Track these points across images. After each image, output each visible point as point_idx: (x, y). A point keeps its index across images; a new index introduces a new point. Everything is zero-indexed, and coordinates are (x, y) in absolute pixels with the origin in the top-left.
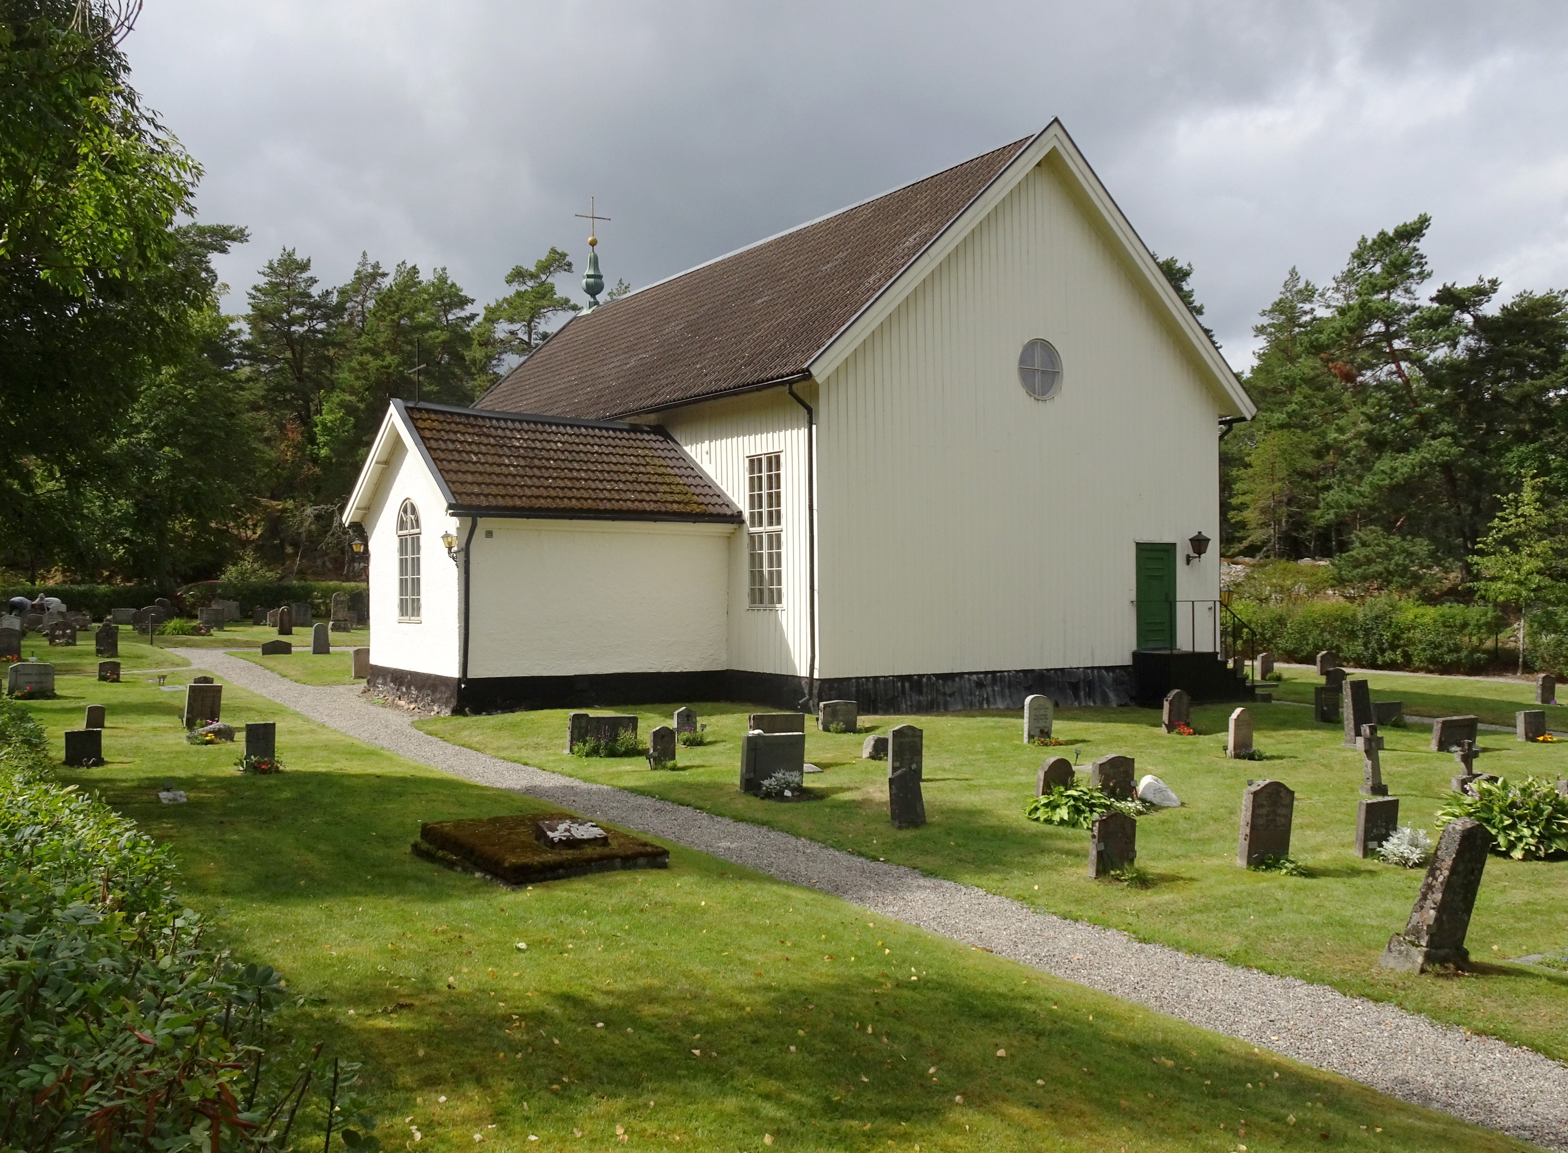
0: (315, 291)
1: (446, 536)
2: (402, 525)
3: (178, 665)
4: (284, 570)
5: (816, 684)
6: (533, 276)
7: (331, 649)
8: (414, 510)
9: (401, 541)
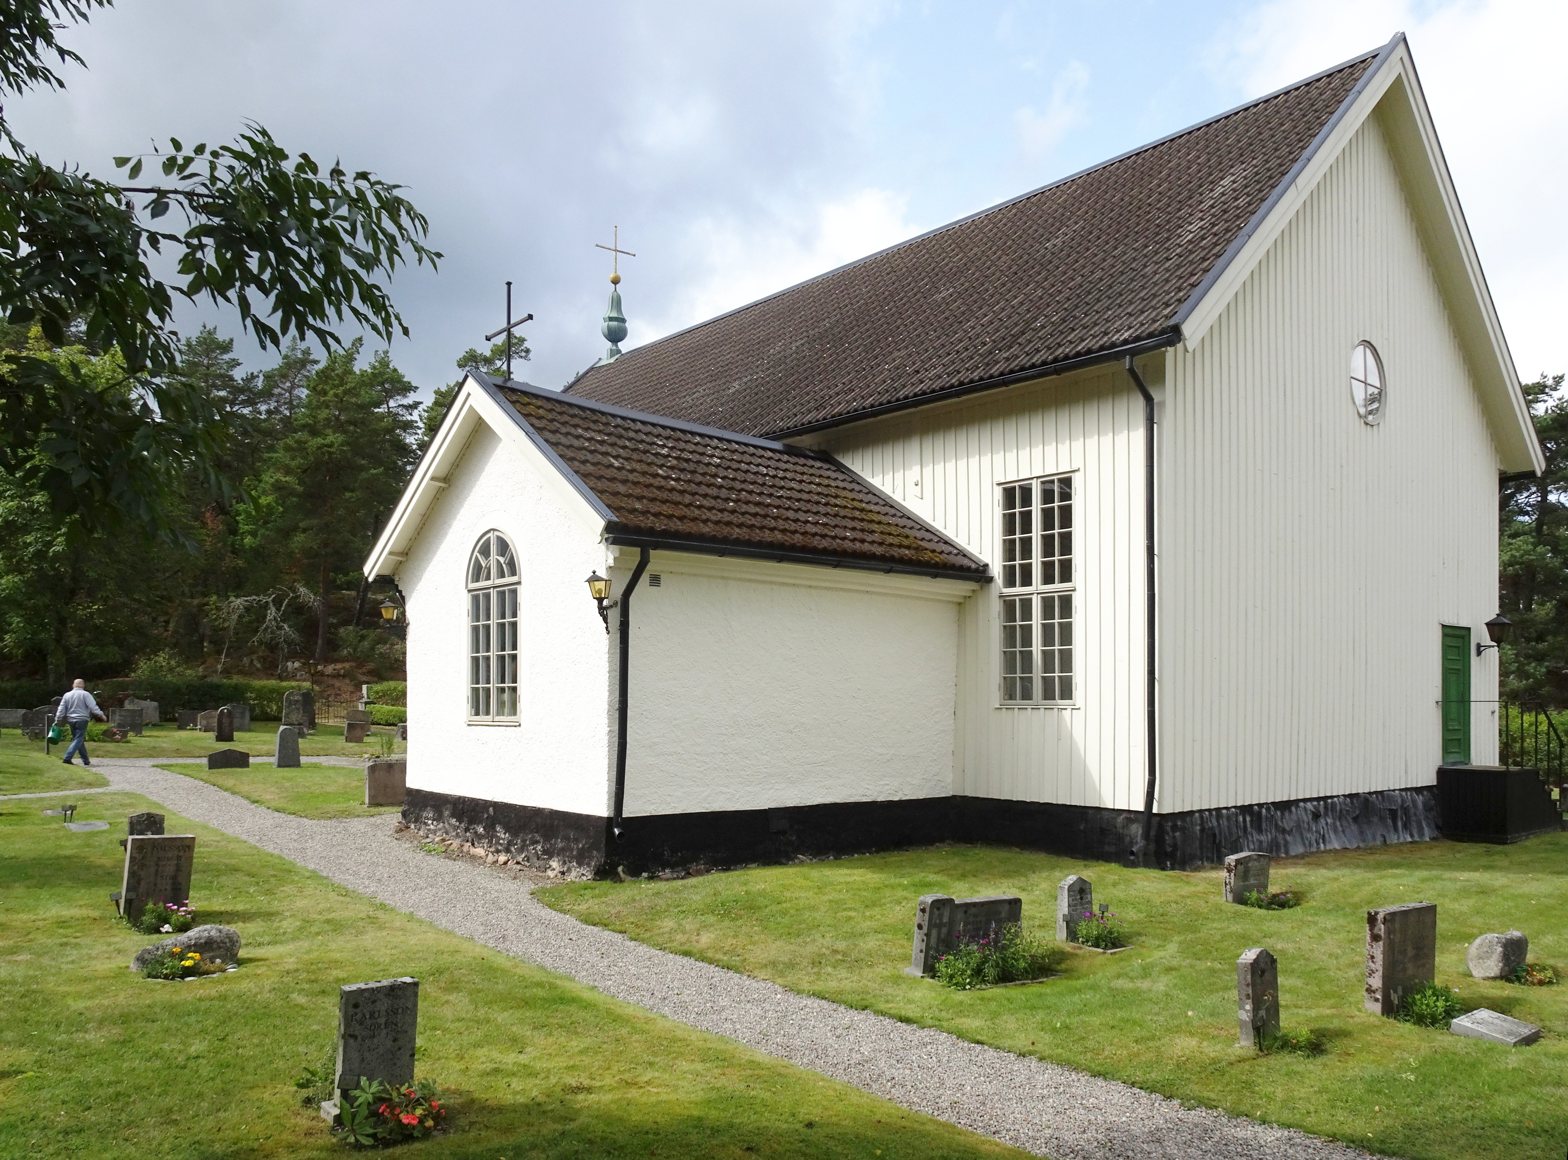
0: (238, 374)
1: (594, 578)
2: (477, 572)
3: (90, 785)
4: (205, 669)
5: (1155, 821)
6: (488, 361)
7: (303, 760)
8: (504, 546)
9: (476, 600)
